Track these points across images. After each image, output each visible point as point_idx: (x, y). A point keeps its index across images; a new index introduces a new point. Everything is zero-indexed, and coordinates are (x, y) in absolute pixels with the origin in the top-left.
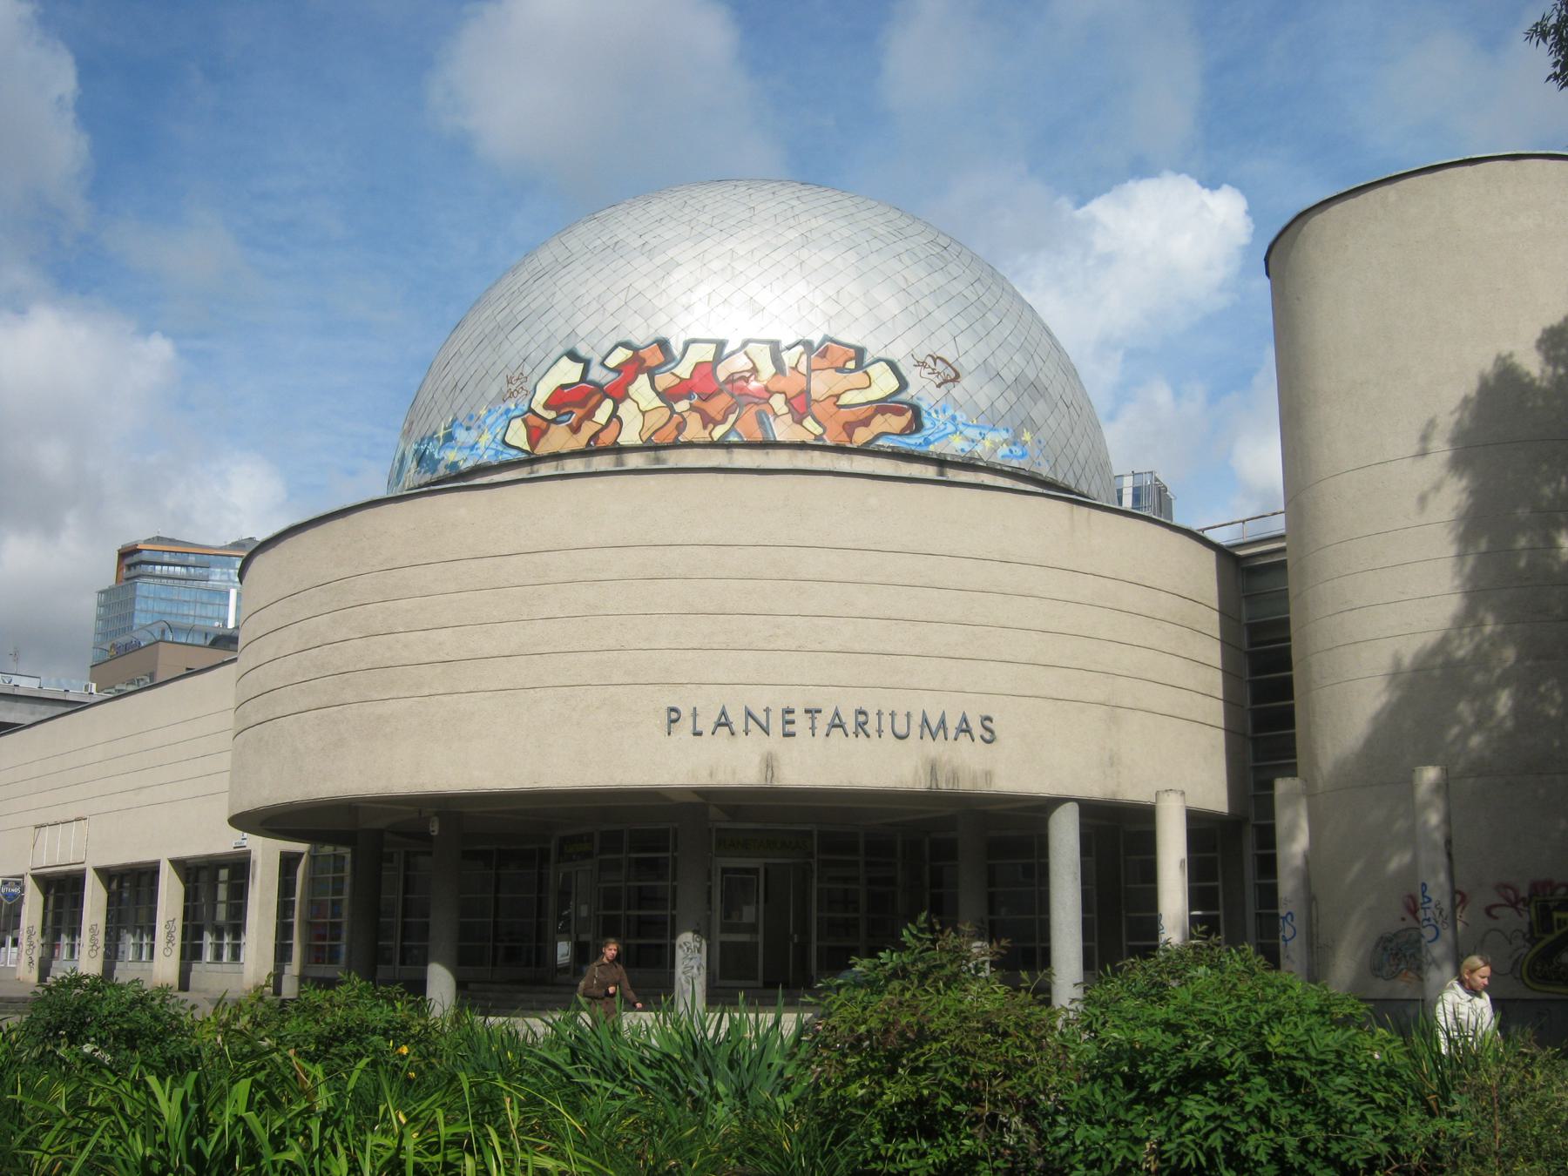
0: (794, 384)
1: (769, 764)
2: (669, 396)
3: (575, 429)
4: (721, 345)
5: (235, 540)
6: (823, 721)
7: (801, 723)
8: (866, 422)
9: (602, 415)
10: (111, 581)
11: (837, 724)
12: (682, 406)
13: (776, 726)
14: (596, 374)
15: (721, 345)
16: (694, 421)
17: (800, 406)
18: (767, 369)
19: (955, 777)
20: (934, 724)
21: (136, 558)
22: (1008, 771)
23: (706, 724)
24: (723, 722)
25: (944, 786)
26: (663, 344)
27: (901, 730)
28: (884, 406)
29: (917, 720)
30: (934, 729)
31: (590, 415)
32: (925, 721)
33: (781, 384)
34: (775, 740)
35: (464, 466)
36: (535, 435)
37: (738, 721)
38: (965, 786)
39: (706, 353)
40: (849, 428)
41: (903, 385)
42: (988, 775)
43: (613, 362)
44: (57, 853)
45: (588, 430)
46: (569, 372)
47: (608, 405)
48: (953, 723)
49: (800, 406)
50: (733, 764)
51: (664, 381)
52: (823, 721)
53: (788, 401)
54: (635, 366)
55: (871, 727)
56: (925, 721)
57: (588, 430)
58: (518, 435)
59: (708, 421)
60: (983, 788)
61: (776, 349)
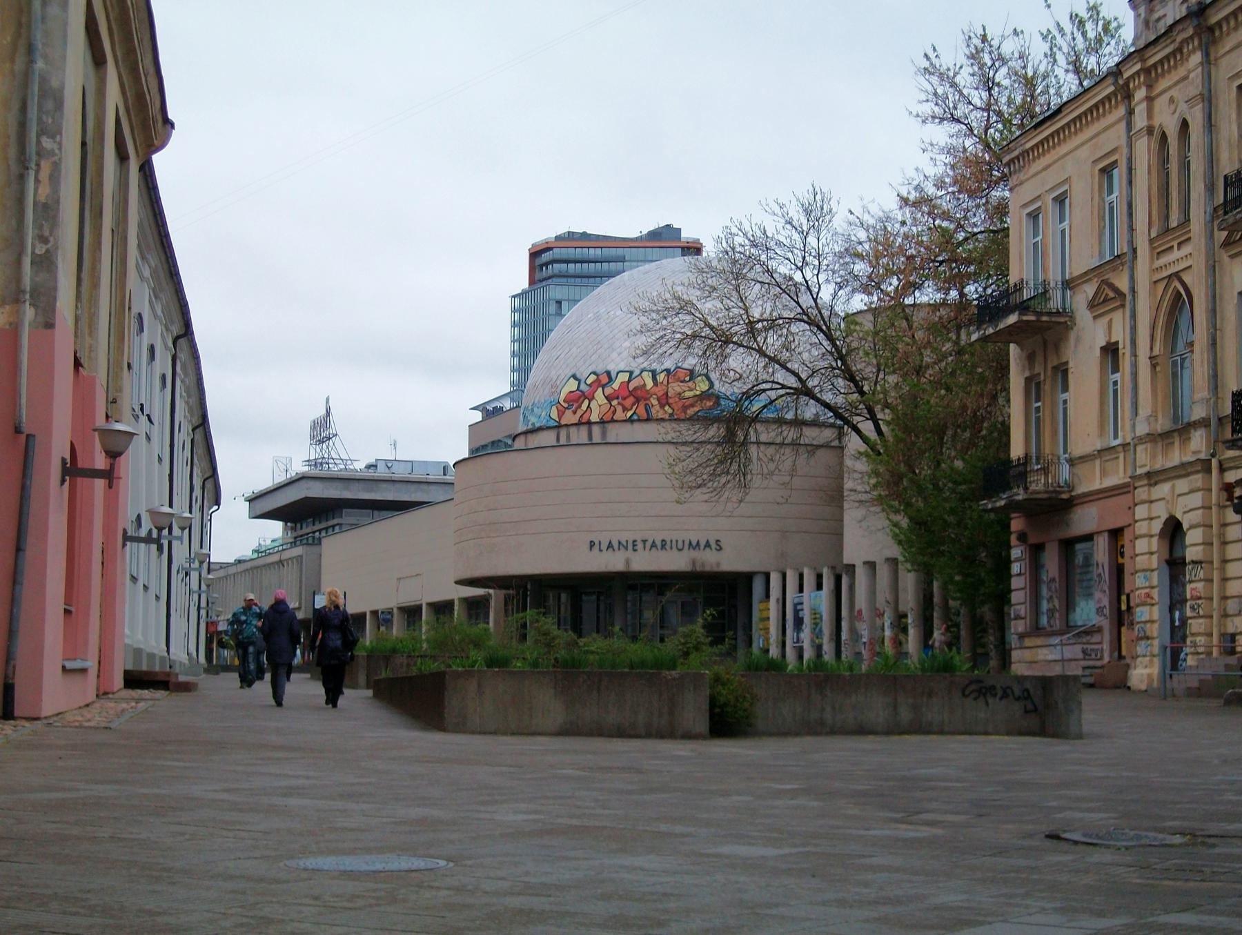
0: (660, 391)
1: (628, 562)
2: (609, 398)
3: (575, 413)
4: (631, 373)
5: (652, 227)
6: (648, 545)
7: (640, 546)
8: (692, 405)
9: (584, 407)
10: (525, 284)
11: (654, 545)
12: (615, 403)
13: (630, 547)
14: (583, 387)
15: (631, 373)
16: (619, 409)
17: (664, 400)
18: (650, 384)
19: (703, 565)
20: (694, 544)
21: (546, 257)
22: (390, 606)
23: (604, 547)
24: (610, 546)
25: (698, 569)
26: (608, 373)
27: (680, 546)
28: (704, 396)
29: (687, 543)
30: (694, 546)
31: (580, 406)
32: (690, 543)
33: (656, 390)
34: (630, 553)
35: (537, 425)
36: (561, 414)
37: (616, 547)
38: (707, 568)
39: (624, 377)
40: (685, 408)
41: (712, 384)
42: (718, 564)
43: (589, 382)
44: (409, 596)
45: (579, 413)
46: (573, 385)
47: (586, 402)
48: (703, 544)
49: (664, 400)
50: (614, 562)
51: (608, 391)
52: (648, 545)
53: (658, 399)
54: (598, 384)
55: (668, 547)
56: (690, 543)
57: (579, 413)
58: (554, 415)
59: (625, 409)
60: (716, 569)
61: (654, 374)
